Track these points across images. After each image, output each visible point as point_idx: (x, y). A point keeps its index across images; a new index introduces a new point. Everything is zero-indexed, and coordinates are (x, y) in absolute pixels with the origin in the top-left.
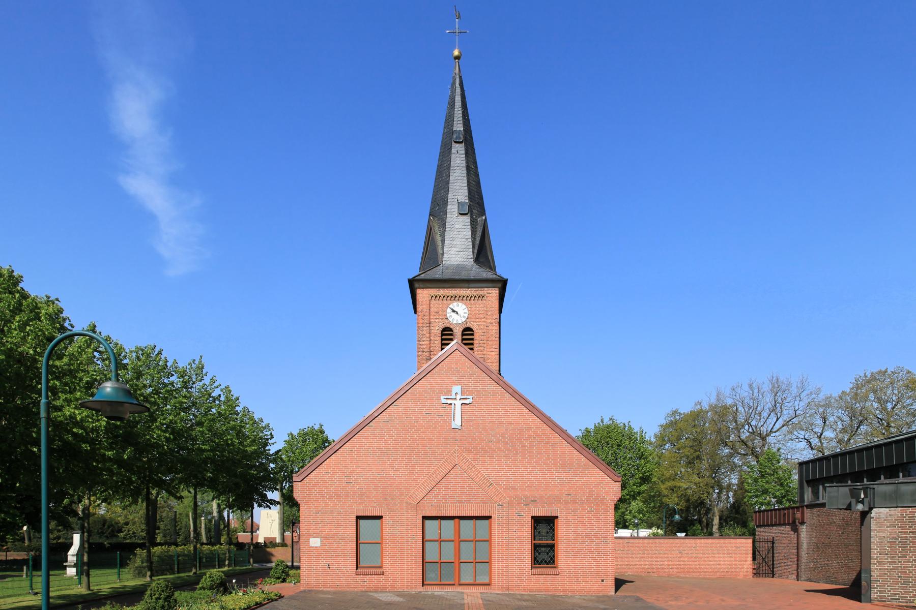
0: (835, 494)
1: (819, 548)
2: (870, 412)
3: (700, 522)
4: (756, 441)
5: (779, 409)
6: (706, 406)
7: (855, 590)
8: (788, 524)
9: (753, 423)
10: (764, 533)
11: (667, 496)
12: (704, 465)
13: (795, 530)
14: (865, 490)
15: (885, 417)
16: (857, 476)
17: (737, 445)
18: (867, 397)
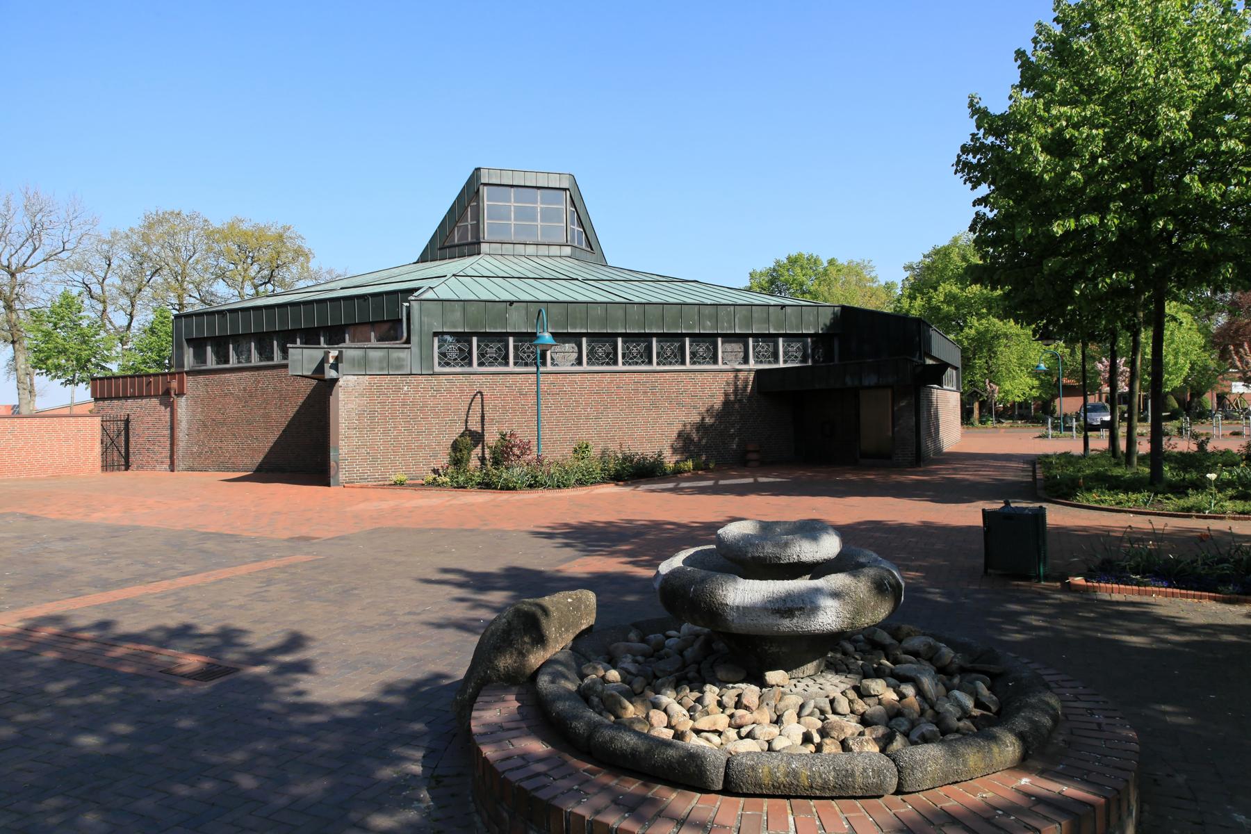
8: (156, 396)
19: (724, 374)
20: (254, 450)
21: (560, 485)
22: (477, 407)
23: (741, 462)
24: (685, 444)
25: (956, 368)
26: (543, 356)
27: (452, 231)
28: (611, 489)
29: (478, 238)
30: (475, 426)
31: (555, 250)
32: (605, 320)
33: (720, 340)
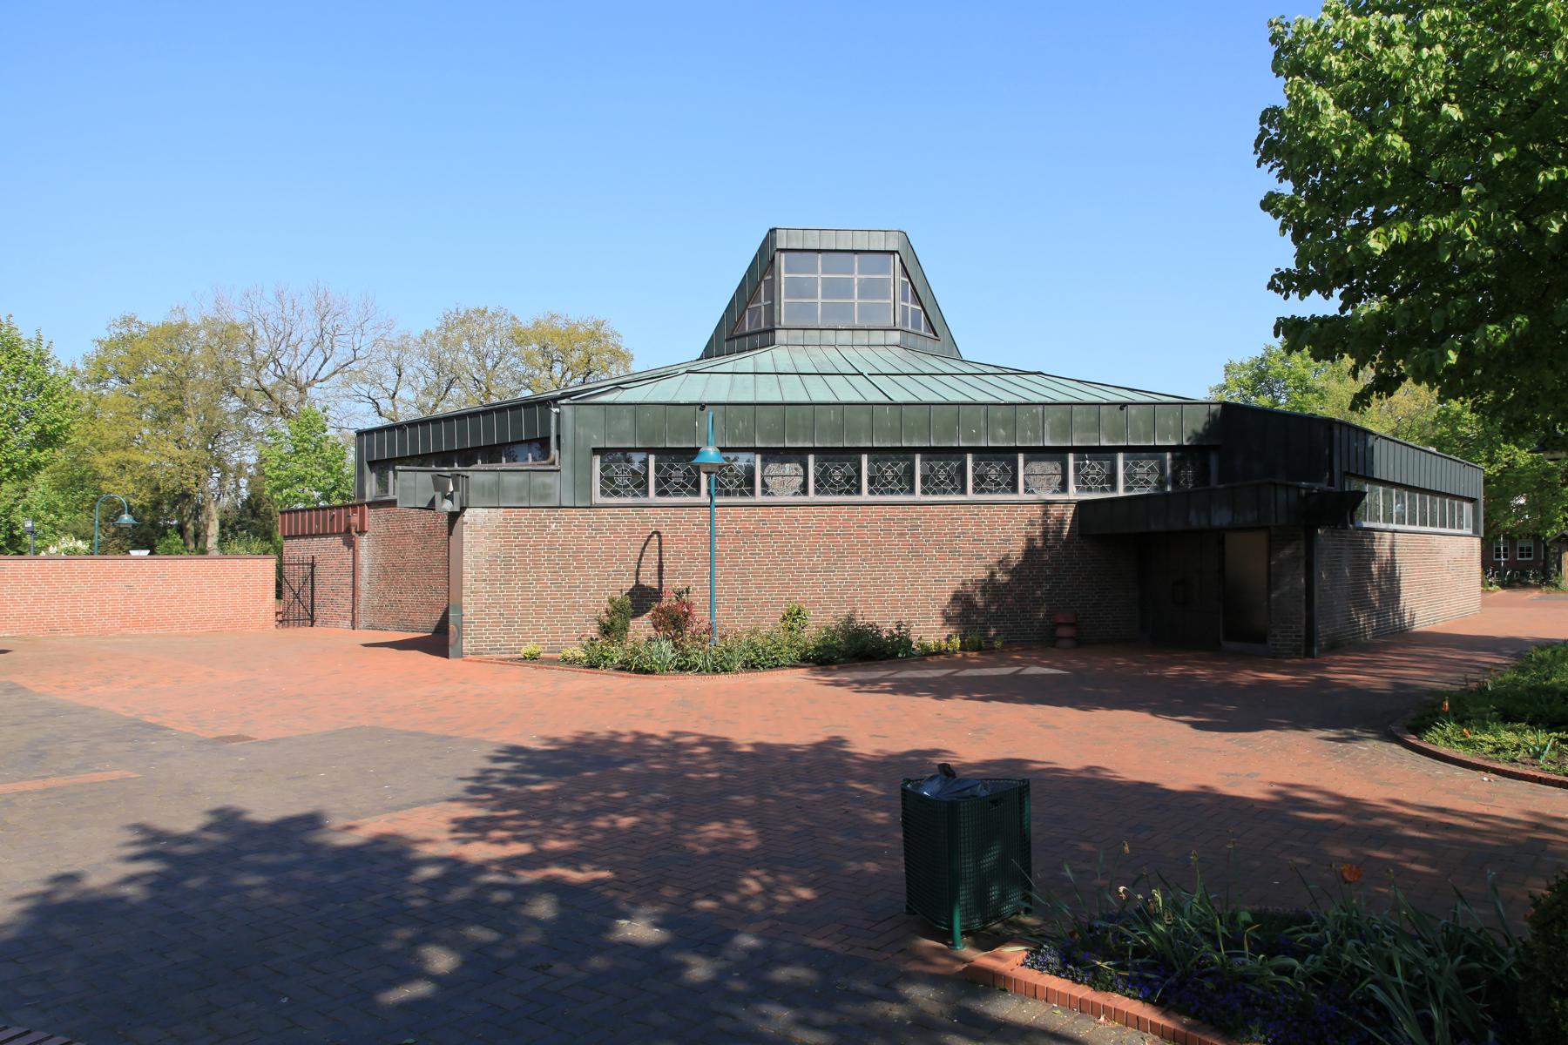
0: (412, 484)
1: (389, 573)
2: (463, 368)
3: (181, 530)
4: (289, 393)
5: (327, 343)
6: (194, 319)
7: (438, 641)
8: (339, 534)
9: (284, 361)
10: (297, 550)
11: (111, 479)
12: (190, 426)
13: (350, 544)
14: (455, 477)
15: (483, 378)
16: (444, 458)
17: (256, 396)
18: (459, 343)
19: (1026, 508)
20: (432, 604)
21: (720, 668)
22: (652, 553)
23: (1046, 641)
24: (963, 610)
25: (1472, 500)
26: (750, 481)
27: (742, 316)
28: (798, 677)
29: (772, 323)
30: (650, 580)
31: (878, 337)
32: (839, 430)
33: (1021, 457)
